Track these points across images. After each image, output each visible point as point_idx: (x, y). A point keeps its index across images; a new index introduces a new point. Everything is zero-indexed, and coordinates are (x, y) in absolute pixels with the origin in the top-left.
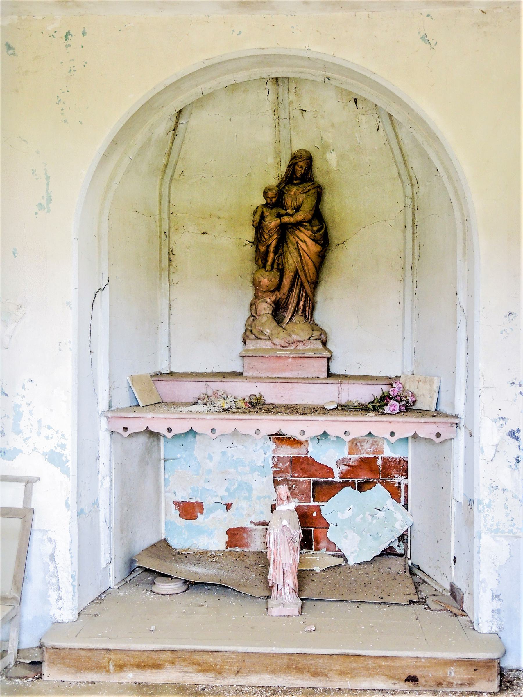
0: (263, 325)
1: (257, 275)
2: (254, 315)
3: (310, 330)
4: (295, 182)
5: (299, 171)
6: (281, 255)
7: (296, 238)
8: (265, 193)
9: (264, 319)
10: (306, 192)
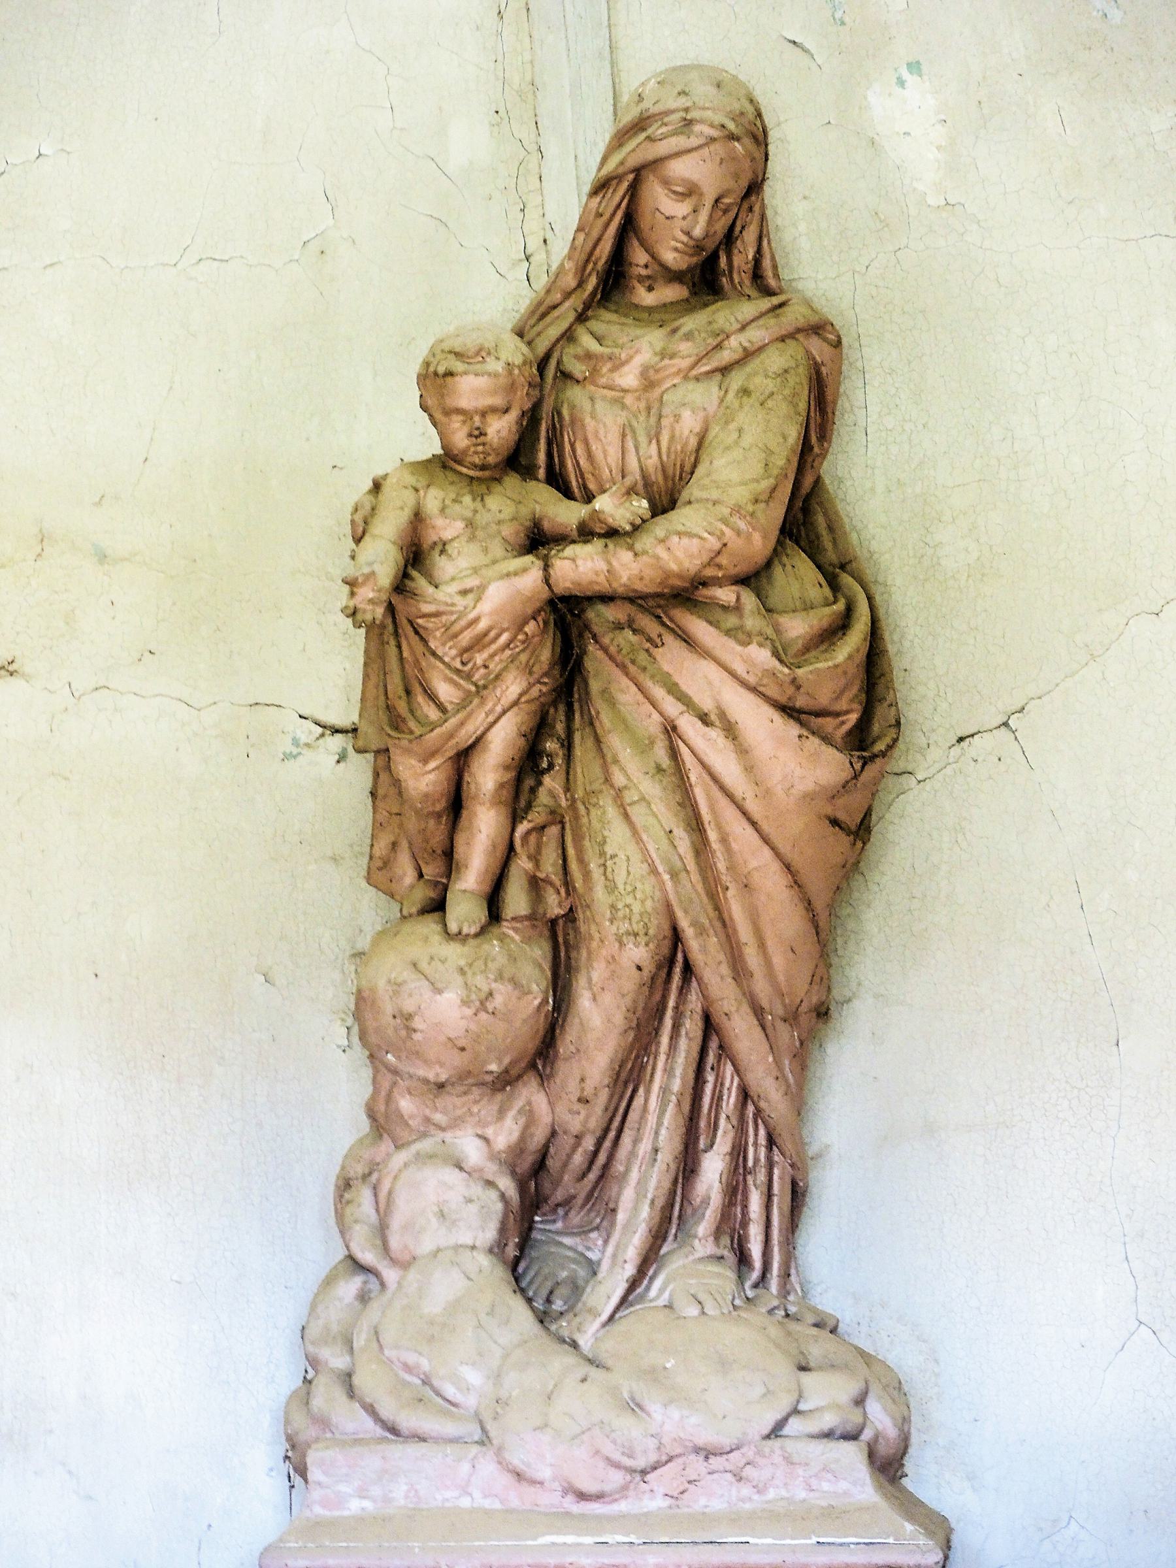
0: (435, 1333)
1: (388, 968)
2: (367, 1257)
3: (783, 1369)
4: (646, 298)
5: (675, 225)
6: (556, 817)
7: (659, 692)
8: (435, 382)
9: (443, 1288)
10: (724, 370)
